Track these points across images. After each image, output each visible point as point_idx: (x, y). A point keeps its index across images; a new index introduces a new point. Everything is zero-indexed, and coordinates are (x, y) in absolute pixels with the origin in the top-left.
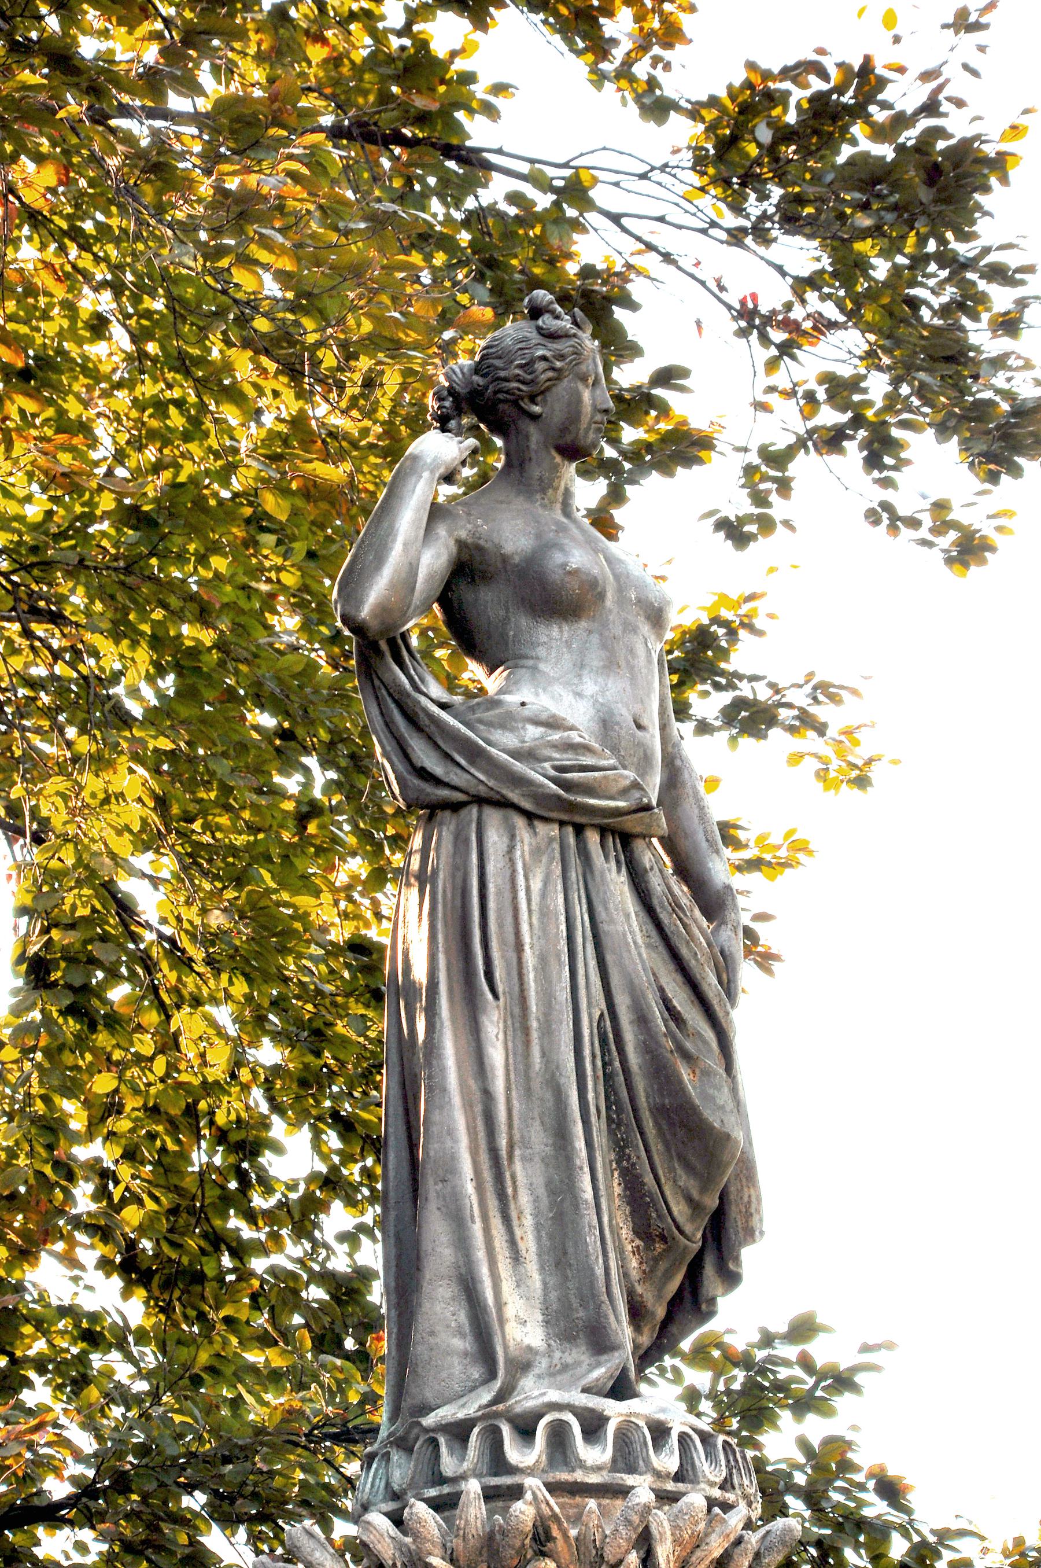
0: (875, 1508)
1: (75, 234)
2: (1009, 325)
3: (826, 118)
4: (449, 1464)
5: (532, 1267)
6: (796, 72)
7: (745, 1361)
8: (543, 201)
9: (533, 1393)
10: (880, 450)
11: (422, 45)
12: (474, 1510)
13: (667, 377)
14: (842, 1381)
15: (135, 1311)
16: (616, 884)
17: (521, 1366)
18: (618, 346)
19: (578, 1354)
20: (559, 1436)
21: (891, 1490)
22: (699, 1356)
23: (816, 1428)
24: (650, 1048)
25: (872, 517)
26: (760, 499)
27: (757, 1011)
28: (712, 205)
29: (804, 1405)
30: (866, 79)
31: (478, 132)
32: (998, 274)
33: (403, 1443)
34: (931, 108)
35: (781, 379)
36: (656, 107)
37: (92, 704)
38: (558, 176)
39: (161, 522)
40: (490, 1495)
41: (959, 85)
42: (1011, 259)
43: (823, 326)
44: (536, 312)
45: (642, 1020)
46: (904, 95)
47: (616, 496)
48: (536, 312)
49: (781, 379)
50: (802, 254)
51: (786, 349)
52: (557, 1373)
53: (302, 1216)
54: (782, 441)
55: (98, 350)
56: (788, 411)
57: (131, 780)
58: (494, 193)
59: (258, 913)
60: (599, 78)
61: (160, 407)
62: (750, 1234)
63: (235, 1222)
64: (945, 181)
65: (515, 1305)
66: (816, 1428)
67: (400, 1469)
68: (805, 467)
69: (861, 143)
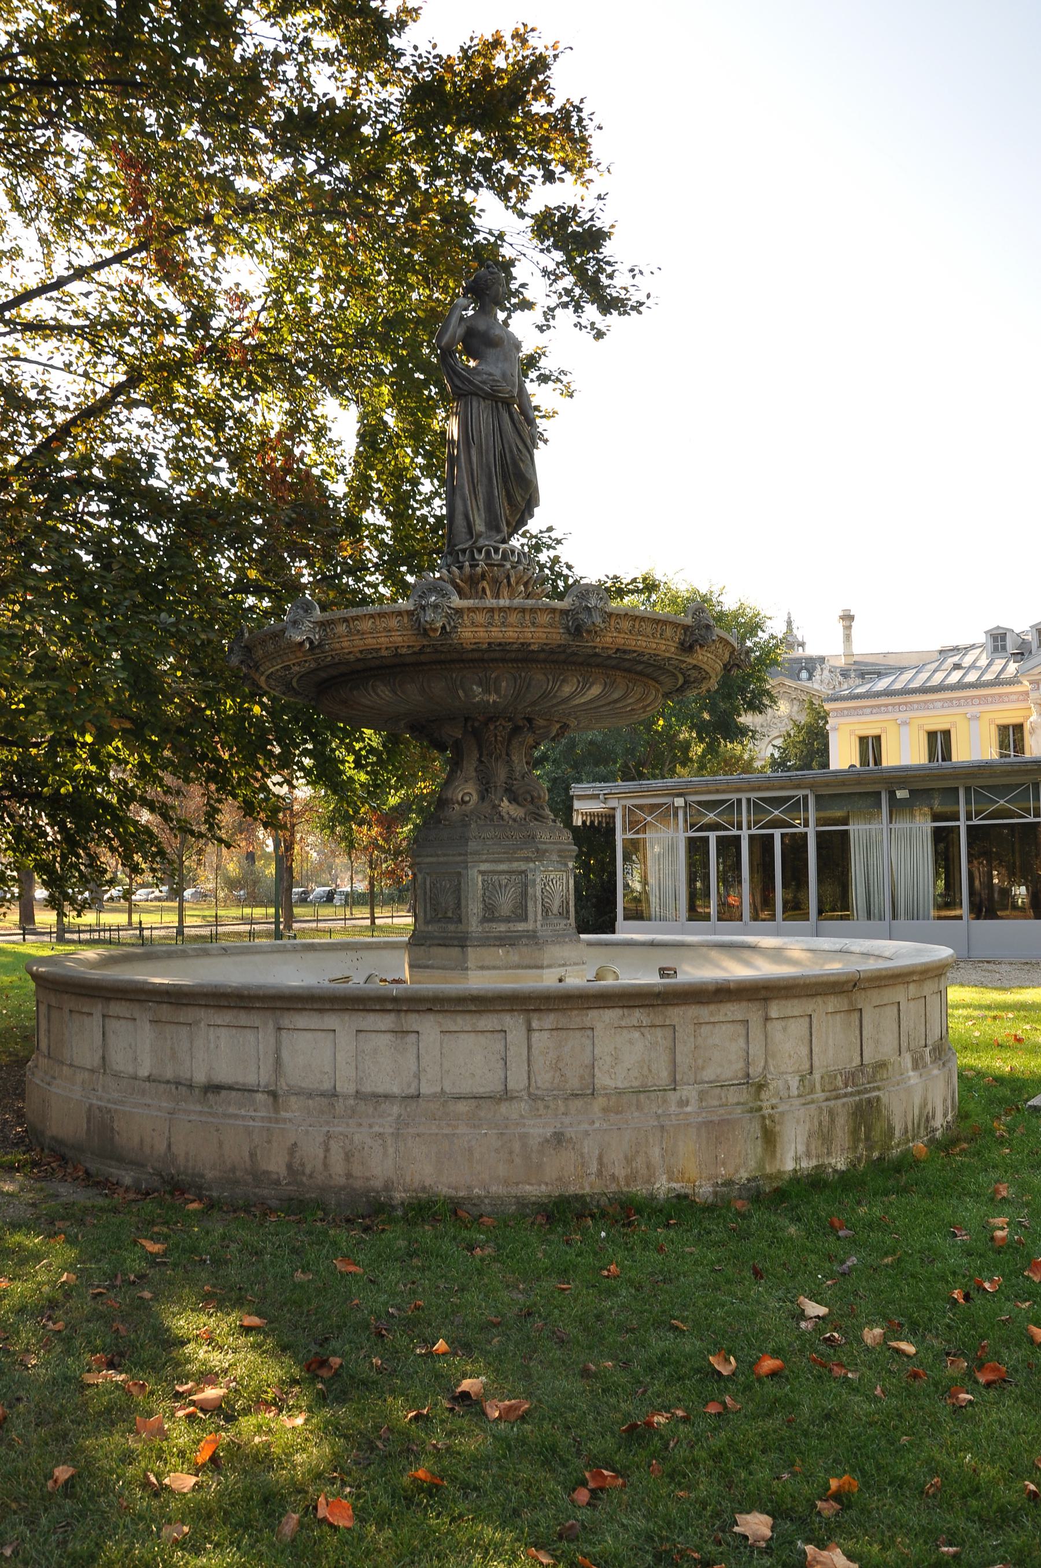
0: (566, 571)
1: (374, 248)
2: (610, 276)
3: (565, 220)
4: (461, 558)
5: (482, 512)
6: (558, 208)
7: (536, 537)
8: (492, 239)
9: (482, 542)
10: (578, 308)
11: (462, 199)
12: (467, 569)
13: (523, 286)
14: (559, 542)
15: (389, 524)
16: (506, 416)
17: (479, 535)
18: (510, 277)
19: (494, 533)
20: (488, 553)
21: (569, 567)
22: (523, 535)
23: (552, 553)
24: (513, 458)
25: (575, 325)
26: (547, 320)
27: (542, 456)
28: (535, 242)
29: (549, 547)
30: (575, 210)
31: (476, 220)
32: (608, 263)
33: (450, 553)
34: (592, 219)
35: (553, 289)
36: (522, 215)
37: (378, 371)
38: (496, 233)
39: (396, 322)
40: (471, 566)
41: (599, 214)
42: (612, 260)
43: (564, 275)
44: (488, 267)
45: (511, 451)
46: (584, 215)
47: (509, 317)
48: (488, 267)
49: (553, 289)
50: (558, 256)
51: (554, 281)
52: (488, 538)
53: (428, 501)
54: (553, 306)
55: (380, 279)
56: (555, 297)
57: (385, 389)
58: (478, 238)
59: (417, 423)
60: (507, 207)
61: (394, 292)
62: (537, 505)
63: (412, 502)
64: (594, 238)
65: (478, 521)
66: (552, 553)
67: (450, 559)
68: (558, 312)
69: (573, 227)
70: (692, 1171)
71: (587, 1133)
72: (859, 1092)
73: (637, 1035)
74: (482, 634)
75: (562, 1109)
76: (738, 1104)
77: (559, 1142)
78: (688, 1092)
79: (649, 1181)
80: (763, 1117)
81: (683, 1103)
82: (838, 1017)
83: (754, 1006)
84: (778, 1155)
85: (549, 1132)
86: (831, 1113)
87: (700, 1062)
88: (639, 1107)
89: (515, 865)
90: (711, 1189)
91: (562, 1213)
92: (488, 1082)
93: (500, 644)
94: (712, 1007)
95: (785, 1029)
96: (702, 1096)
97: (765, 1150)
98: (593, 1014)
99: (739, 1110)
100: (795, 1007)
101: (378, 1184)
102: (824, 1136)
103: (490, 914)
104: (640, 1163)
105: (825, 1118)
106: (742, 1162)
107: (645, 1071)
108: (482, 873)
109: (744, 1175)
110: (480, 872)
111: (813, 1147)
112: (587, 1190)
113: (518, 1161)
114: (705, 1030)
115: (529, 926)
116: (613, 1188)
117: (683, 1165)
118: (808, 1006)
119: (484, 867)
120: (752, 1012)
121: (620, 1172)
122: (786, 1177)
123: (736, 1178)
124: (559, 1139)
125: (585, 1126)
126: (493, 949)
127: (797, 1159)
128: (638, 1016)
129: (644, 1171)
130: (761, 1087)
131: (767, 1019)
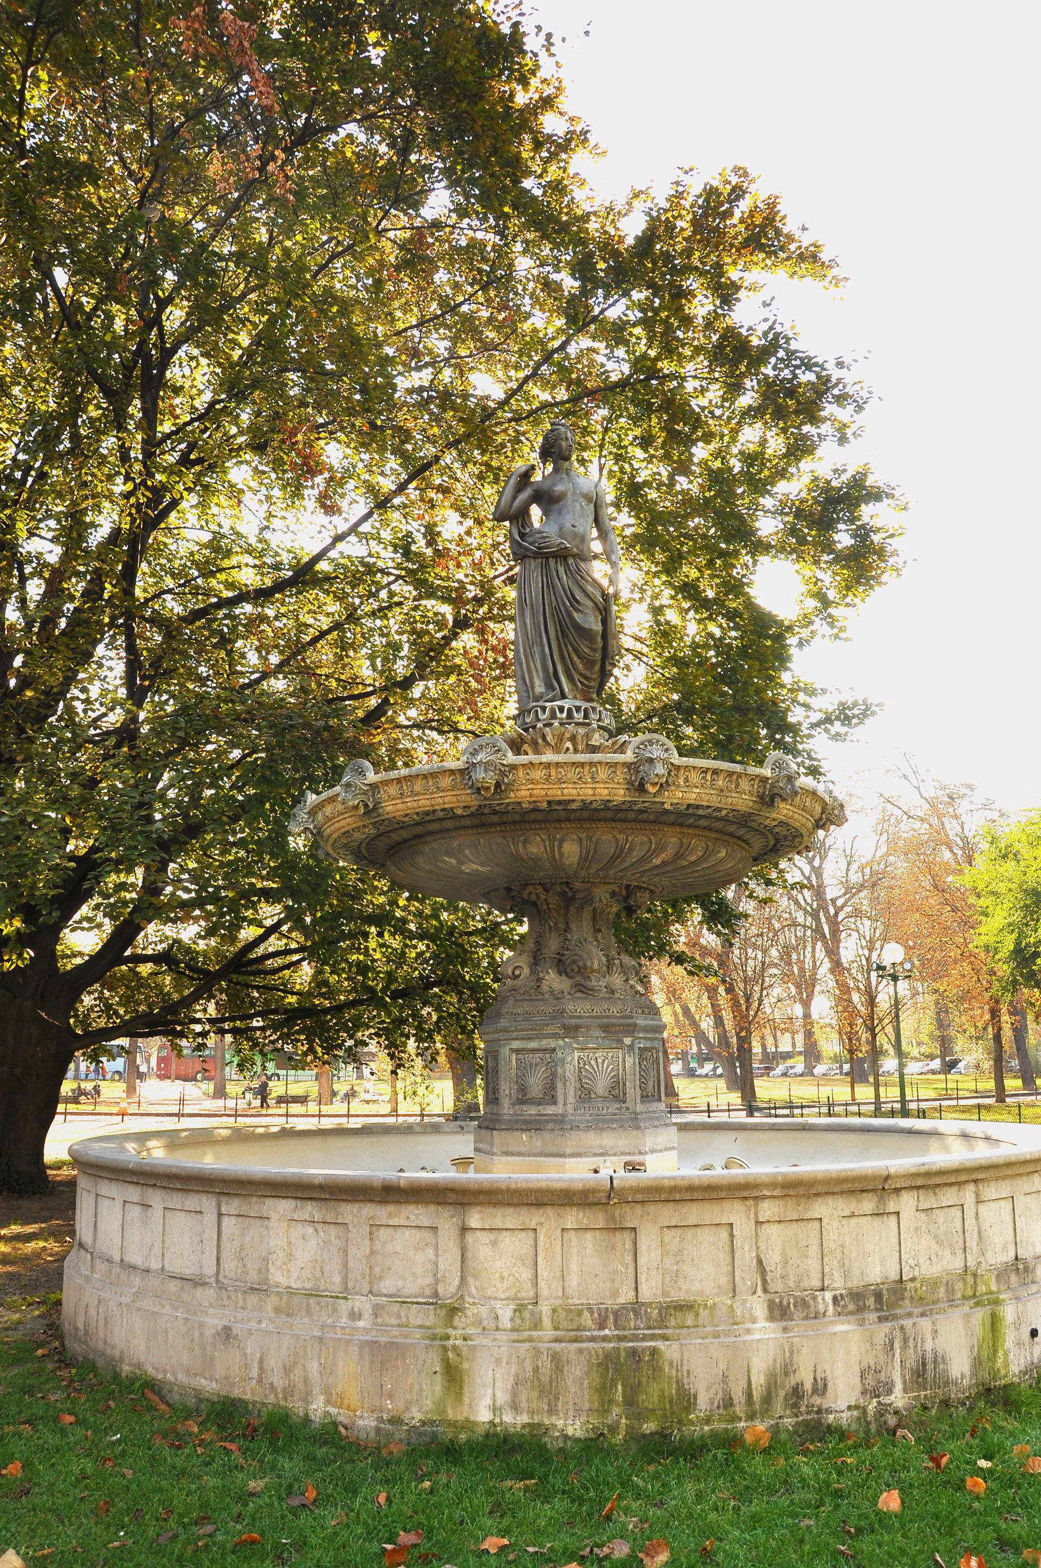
70: (353, 1397)
71: (250, 1333)
72: (620, 1339)
73: (310, 1230)
74: (539, 792)
75: (241, 1303)
76: (422, 1327)
77: (228, 1336)
78: (361, 1303)
79: (306, 1400)
80: (445, 1349)
81: (355, 1315)
82: (589, 1236)
83: (445, 1212)
84: (466, 1400)
85: (220, 1324)
86: (555, 1357)
87: (377, 1270)
88: (309, 1312)
89: (545, 1043)
90: (373, 1424)
91: (227, 1415)
92: (183, 1263)
93: (560, 802)
94: (391, 1208)
95: (494, 1244)
96: (377, 1311)
97: (447, 1390)
98: (269, 1202)
99: (418, 1334)
100: (507, 1218)
101: (117, 1353)
102: (548, 1389)
103: (523, 1098)
104: (297, 1375)
105: (546, 1365)
106: (417, 1399)
107: (318, 1274)
108: (517, 1051)
109: (415, 1416)
110: (512, 1050)
111: (524, 1398)
112: (248, 1397)
113: (197, 1350)
114: (383, 1234)
115: (558, 1109)
116: (271, 1399)
117: (341, 1389)
118: (533, 1218)
119: (516, 1044)
120: (446, 1221)
121: (280, 1383)
122: (481, 1430)
123: (406, 1417)
124: (227, 1334)
125: (253, 1325)
126: (518, 1134)
127: (495, 1409)
128: (310, 1210)
129: (301, 1386)
130: (453, 1311)
131: (464, 1229)
